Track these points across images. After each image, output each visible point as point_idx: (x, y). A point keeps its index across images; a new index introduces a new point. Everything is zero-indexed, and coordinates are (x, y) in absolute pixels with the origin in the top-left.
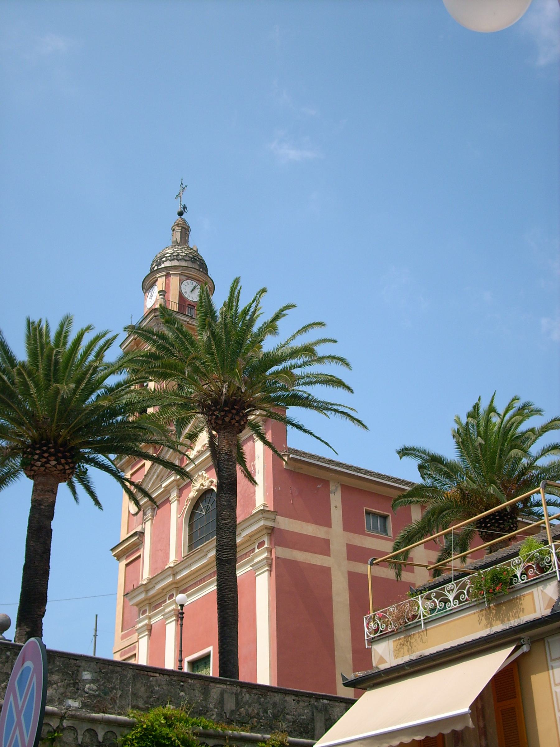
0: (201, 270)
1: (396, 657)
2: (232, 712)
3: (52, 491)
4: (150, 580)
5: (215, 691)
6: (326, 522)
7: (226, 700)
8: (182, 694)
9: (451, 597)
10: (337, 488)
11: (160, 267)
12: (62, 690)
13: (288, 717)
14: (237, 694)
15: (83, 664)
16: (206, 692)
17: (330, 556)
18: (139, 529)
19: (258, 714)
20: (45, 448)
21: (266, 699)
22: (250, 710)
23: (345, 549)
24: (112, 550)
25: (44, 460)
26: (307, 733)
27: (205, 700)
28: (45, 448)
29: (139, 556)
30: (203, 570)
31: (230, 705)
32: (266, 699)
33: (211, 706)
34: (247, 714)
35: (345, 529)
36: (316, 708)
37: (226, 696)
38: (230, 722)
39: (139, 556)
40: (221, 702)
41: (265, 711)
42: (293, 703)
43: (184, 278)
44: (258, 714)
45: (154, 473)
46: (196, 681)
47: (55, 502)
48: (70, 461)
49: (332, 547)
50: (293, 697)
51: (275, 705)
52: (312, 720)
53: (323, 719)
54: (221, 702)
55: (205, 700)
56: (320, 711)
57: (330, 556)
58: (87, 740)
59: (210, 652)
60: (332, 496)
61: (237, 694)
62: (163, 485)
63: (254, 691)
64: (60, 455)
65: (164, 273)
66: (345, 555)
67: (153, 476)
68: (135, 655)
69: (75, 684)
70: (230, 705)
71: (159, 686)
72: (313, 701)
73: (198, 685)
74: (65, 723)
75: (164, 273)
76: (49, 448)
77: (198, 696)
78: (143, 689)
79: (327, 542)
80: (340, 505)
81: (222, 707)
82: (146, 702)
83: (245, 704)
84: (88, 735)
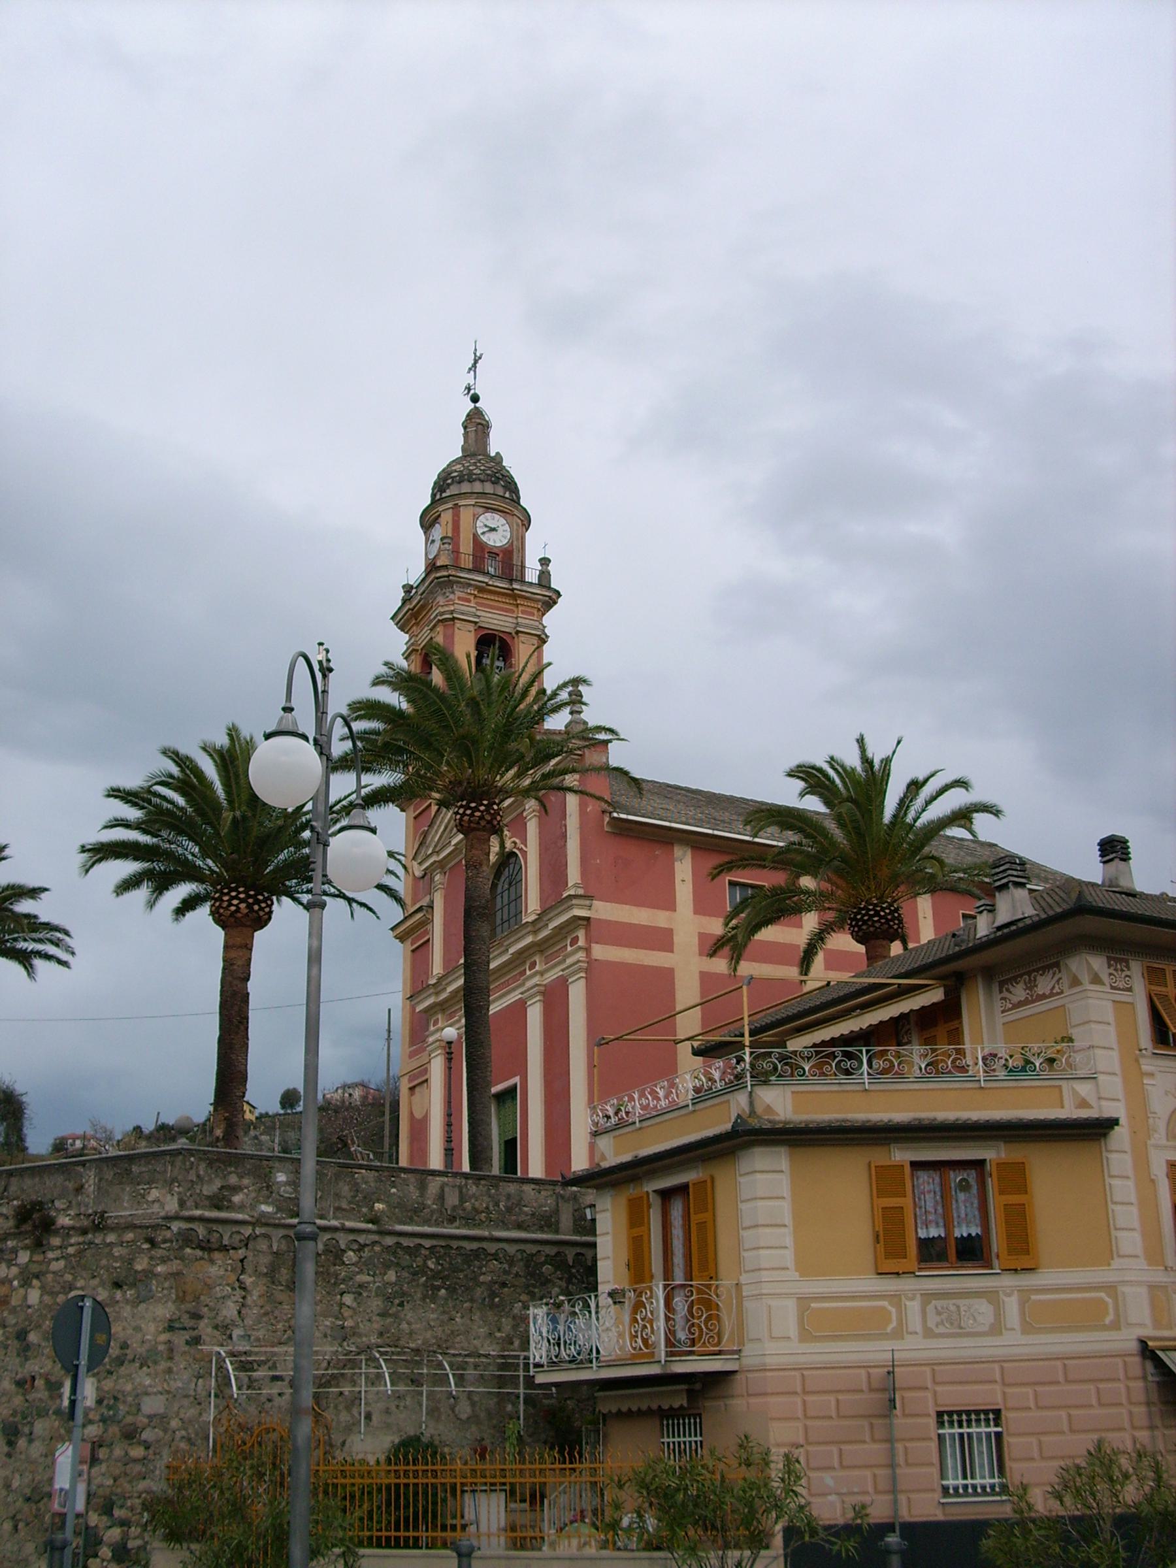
0: (507, 495)
1: (616, 1154)
2: (454, 1208)
3: (246, 946)
4: (440, 979)
5: (434, 1185)
6: (669, 904)
7: (446, 1195)
8: (393, 1190)
9: (661, 1093)
10: (684, 855)
11: (444, 495)
12: (253, 1195)
13: (525, 1209)
14: (460, 1187)
15: (277, 1164)
16: (422, 1187)
17: (672, 951)
18: (425, 902)
19: (487, 1208)
20: (234, 894)
21: (497, 1190)
22: (477, 1204)
23: (696, 940)
24: (392, 929)
25: (233, 908)
26: (549, 1226)
27: (422, 1195)
28: (234, 894)
29: (428, 940)
30: (507, 969)
31: (452, 1199)
32: (497, 1190)
33: (429, 1202)
34: (474, 1208)
35: (696, 912)
36: (562, 1197)
37: (447, 1189)
38: (452, 1220)
39: (428, 940)
40: (441, 1197)
41: (497, 1204)
42: (532, 1193)
43: (481, 510)
44: (487, 1208)
45: (441, 822)
46: (410, 1176)
47: (250, 959)
48: (263, 905)
49: (676, 939)
50: (533, 1186)
51: (509, 1196)
52: (556, 1211)
53: (571, 1210)
54: (441, 1197)
55: (422, 1195)
56: (568, 1201)
57: (672, 951)
58: (284, 1247)
59: (516, 1085)
60: (677, 865)
61: (460, 1187)
62: (453, 843)
63: (483, 1182)
64: (251, 901)
65: (450, 505)
66: (696, 949)
67: (439, 826)
68: (426, 1081)
69: (268, 1187)
70: (452, 1199)
71: (366, 1183)
72: (559, 1189)
73: (413, 1180)
74: (258, 1231)
75: (450, 505)
76: (240, 893)
77: (413, 1192)
78: (346, 1188)
79: (669, 933)
80: (689, 876)
81: (443, 1204)
82: (350, 1203)
83: (470, 1198)
84: (284, 1242)
